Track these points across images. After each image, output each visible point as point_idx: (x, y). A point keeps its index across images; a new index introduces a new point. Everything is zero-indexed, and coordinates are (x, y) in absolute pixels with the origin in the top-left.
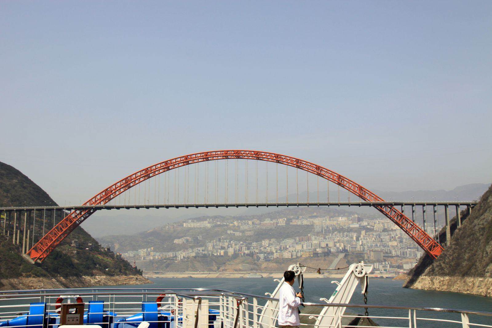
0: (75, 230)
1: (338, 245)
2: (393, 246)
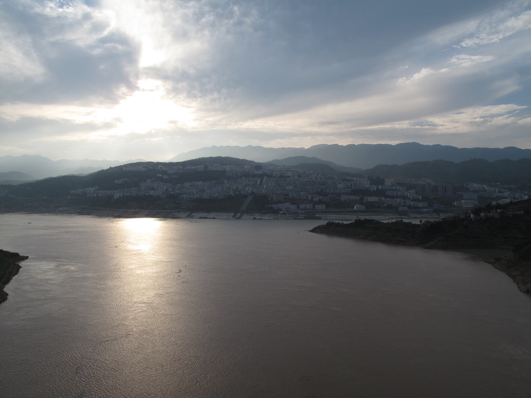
0: (317, 205)
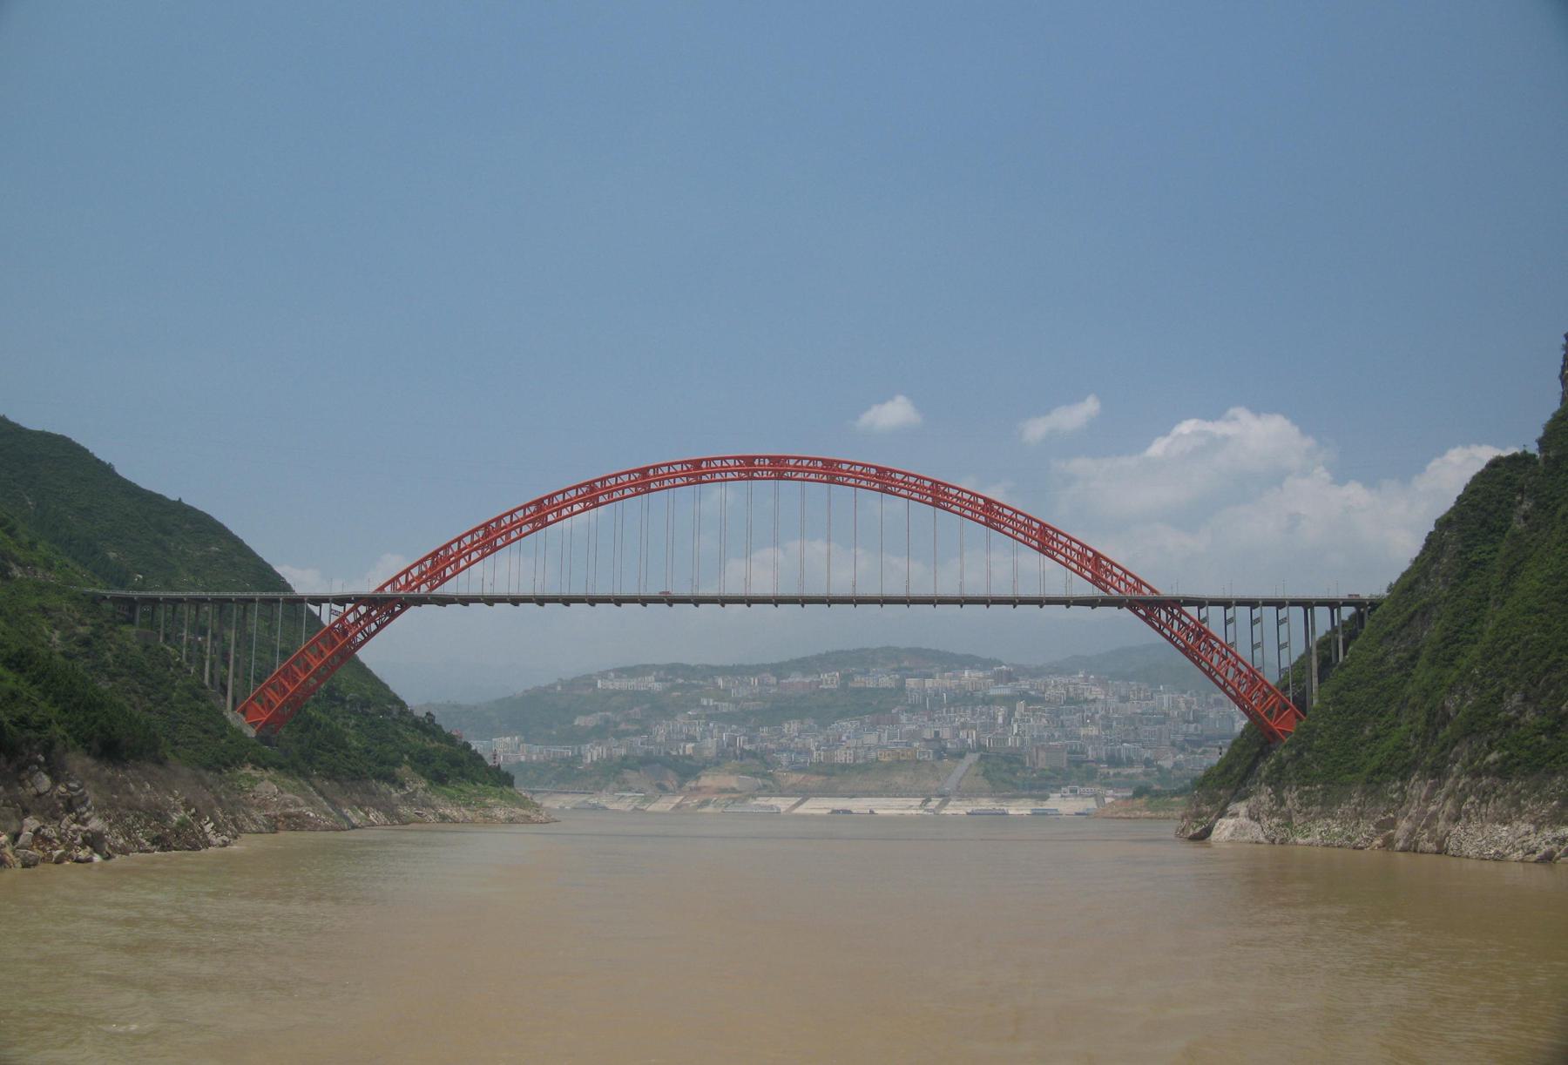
1: (963, 734)
2: (1088, 737)
